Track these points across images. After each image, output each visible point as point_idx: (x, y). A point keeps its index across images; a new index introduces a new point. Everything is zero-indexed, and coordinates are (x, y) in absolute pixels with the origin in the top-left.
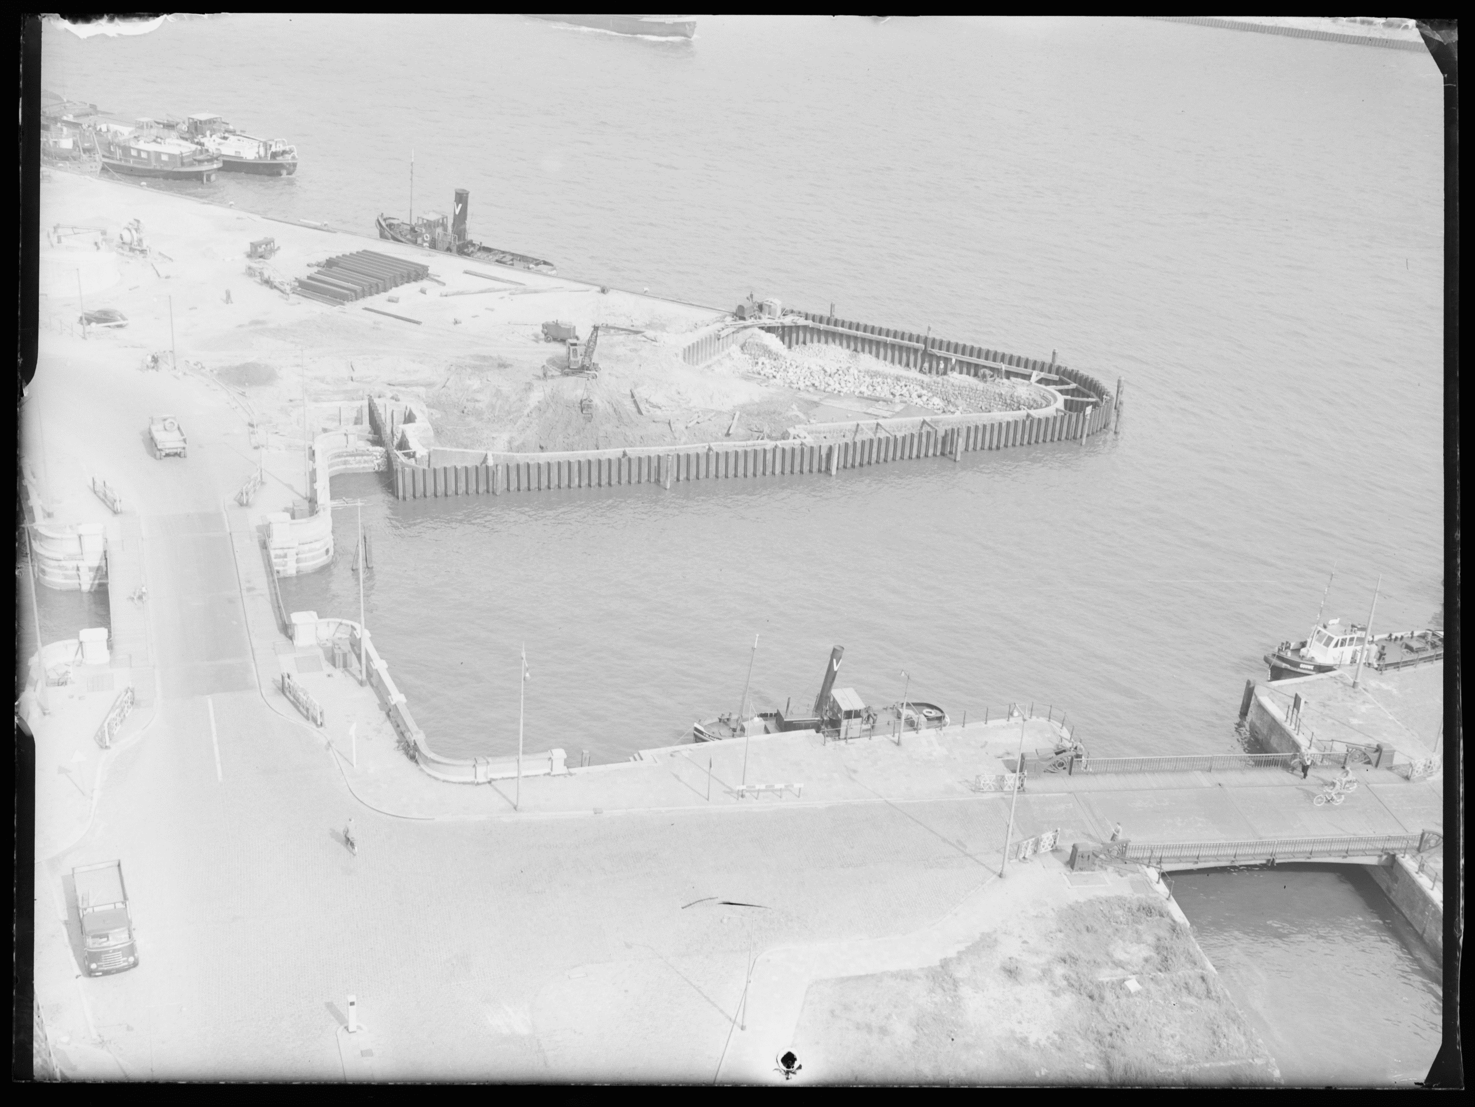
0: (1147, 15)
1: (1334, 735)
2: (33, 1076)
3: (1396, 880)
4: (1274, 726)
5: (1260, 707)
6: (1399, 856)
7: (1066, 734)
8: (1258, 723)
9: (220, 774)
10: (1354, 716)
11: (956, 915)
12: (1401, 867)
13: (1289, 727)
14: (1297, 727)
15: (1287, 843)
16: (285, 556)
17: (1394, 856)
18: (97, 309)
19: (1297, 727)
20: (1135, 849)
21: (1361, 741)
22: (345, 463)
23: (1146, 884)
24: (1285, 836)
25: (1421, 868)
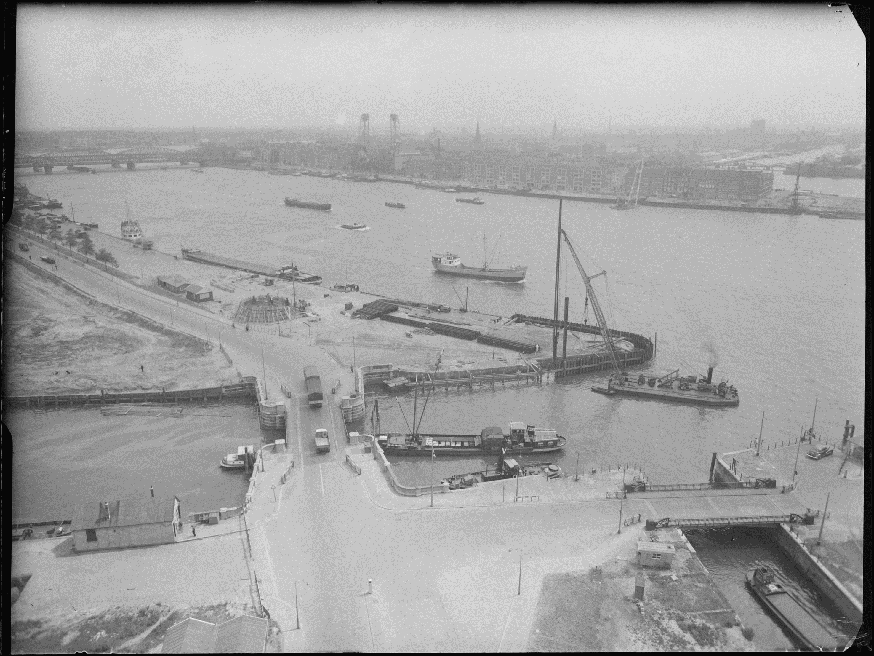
0: (358, 654)
1: (750, 475)
2: (852, 9)
3: (781, 534)
4: (725, 471)
5: (719, 464)
6: (782, 524)
7: (642, 476)
8: (719, 472)
9: (323, 493)
10: (758, 467)
11: (601, 548)
12: (783, 528)
13: (732, 472)
14: (735, 472)
15: (734, 519)
16: (348, 411)
17: (779, 524)
18: (795, 162)
19: (735, 472)
20: (673, 521)
21: (763, 477)
22: (369, 377)
23: (677, 536)
24: (733, 515)
25: (792, 529)
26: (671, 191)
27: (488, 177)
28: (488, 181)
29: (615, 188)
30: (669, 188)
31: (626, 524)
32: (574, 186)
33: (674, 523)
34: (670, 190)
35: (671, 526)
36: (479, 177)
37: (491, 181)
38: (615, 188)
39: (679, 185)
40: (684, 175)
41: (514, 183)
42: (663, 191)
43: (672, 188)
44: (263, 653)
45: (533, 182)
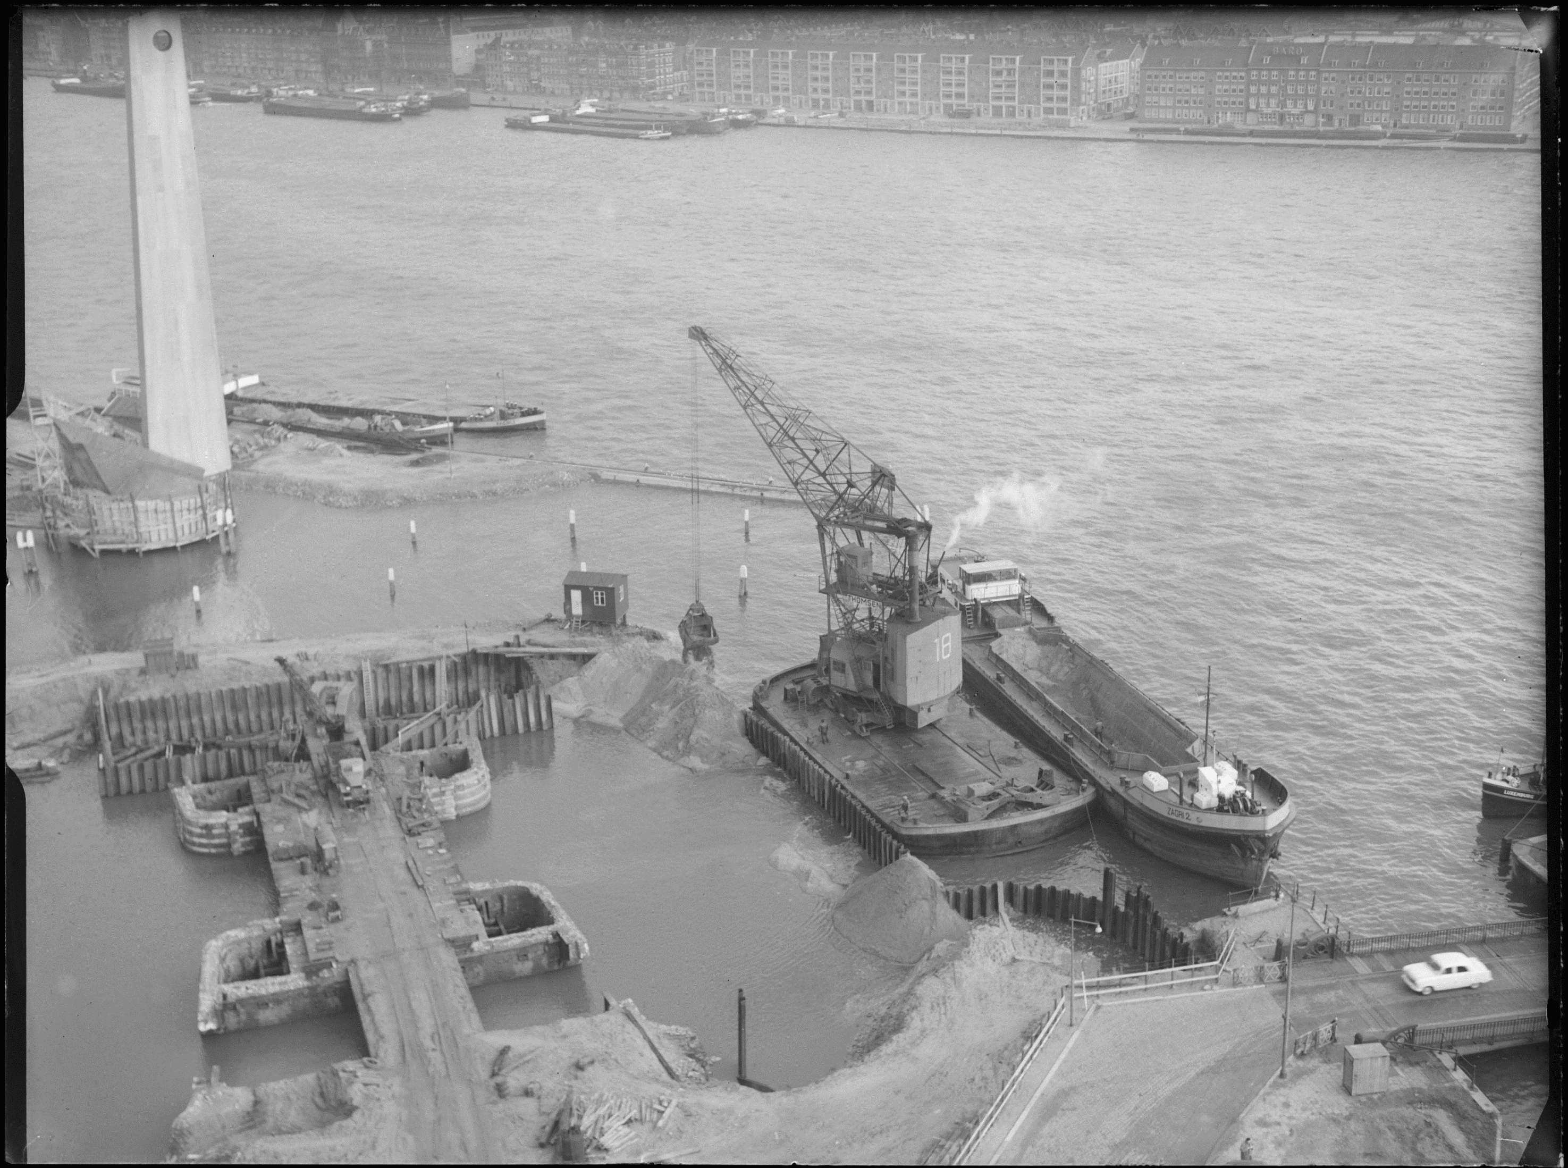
20: (1425, 1032)
26: (1269, 111)
27: (738, 87)
28: (738, 97)
29: (1109, 105)
30: (1262, 101)
31: (1299, 1051)
32: (992, 103)
33: (1428, 1039)
34: (1268, 105)
35: (1423, 1047)
36: (748, 87)
37: (748, 98)
38: (1109, 105)
39: (1253, 89)
40: (1304, 60)
41: (1049, 111)
42: (1248, 110)
43: (1273, 102)
44: (8, 523)
45: (873, 98)
